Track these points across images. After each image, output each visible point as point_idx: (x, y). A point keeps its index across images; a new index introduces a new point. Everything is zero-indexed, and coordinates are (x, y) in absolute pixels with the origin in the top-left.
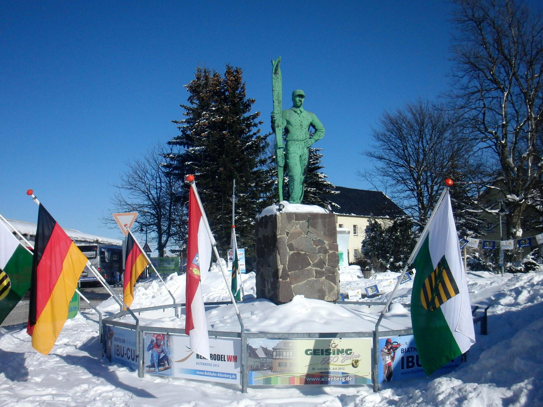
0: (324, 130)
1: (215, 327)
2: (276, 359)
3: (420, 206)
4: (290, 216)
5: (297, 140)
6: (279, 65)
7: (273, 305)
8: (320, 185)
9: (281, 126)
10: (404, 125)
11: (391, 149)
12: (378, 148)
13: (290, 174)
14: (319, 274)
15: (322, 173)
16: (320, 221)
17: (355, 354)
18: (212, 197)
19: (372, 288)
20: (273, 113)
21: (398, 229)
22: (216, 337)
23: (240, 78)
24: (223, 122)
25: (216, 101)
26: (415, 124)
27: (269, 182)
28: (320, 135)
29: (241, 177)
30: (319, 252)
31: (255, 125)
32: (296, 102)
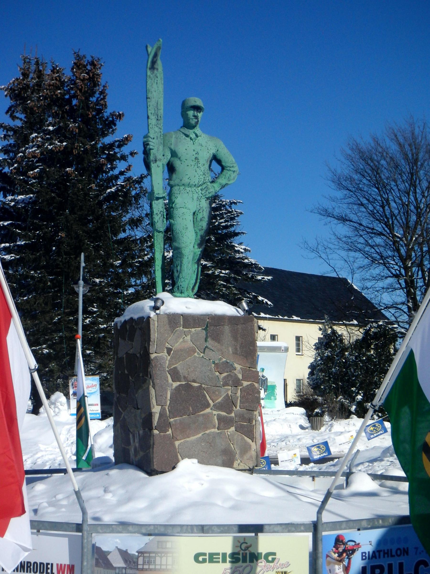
0: (236, 168)
1: (40, 512)
2: (142, 569)
3: (410, 304)
4: (174, 319)
5: (189, 185)
6: (160, 54)
7: (142, 475)
8: (237, 266)
9: (160, 160)
10: (383, 162)
11: (362, 204)
12: (335, 198)
13: (175, 244)
14: (224, 423)
15: (241, 244)
16: (227, 329)
17: (281, 562)
18: (45, 283)
19: (319, 447)
20: (146, 136)
21: (371, 344)
22: (38, 531)
23: (98, 75)
24: (67, 151)
25: (55, 115)
26: (403, 161)
27: (146, 258)
28: (230, 177)
29: (97, 249)
31: (124, 158)
32: (187, 118)
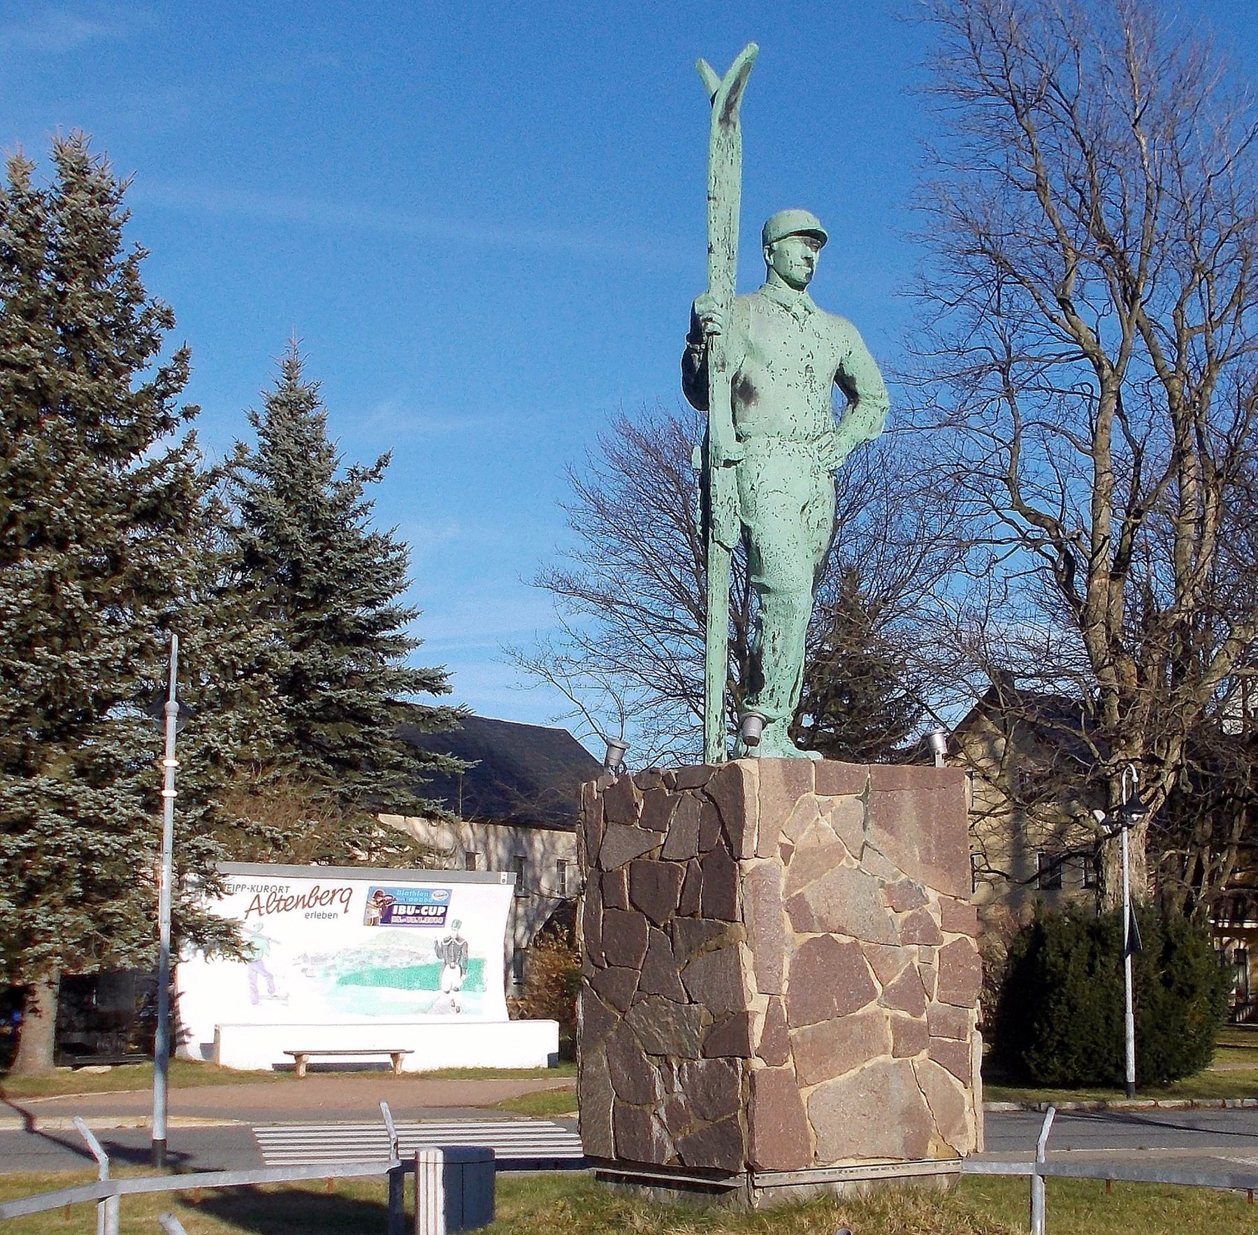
12: (572, 548)
14: (909, 1038)
30: (907, 940)
